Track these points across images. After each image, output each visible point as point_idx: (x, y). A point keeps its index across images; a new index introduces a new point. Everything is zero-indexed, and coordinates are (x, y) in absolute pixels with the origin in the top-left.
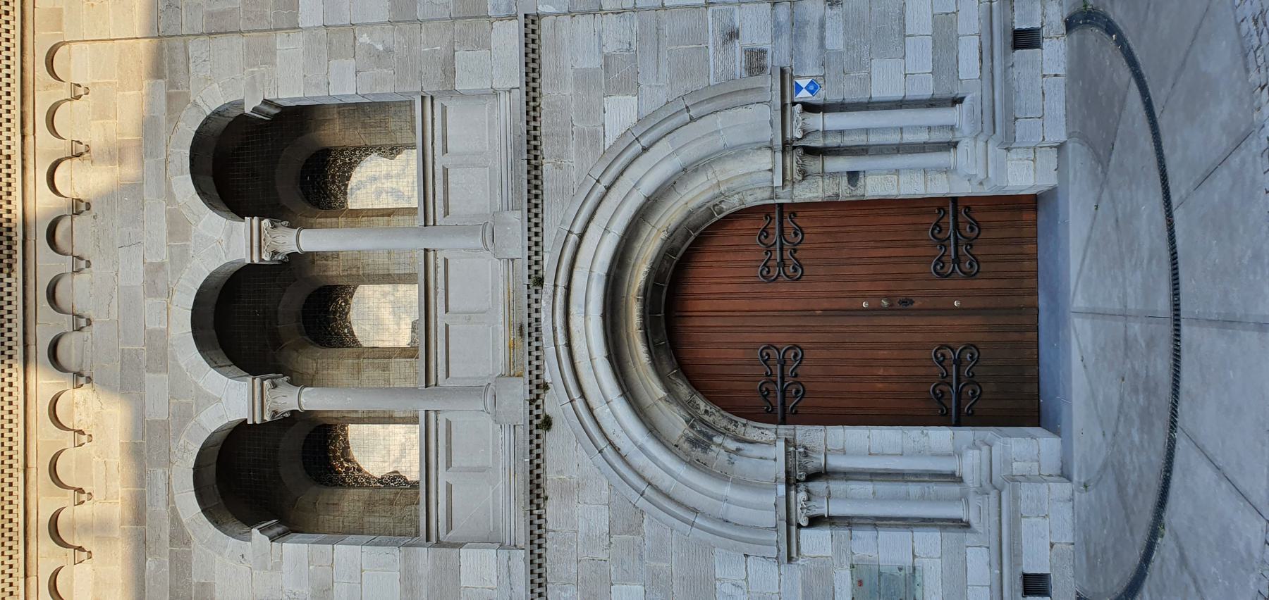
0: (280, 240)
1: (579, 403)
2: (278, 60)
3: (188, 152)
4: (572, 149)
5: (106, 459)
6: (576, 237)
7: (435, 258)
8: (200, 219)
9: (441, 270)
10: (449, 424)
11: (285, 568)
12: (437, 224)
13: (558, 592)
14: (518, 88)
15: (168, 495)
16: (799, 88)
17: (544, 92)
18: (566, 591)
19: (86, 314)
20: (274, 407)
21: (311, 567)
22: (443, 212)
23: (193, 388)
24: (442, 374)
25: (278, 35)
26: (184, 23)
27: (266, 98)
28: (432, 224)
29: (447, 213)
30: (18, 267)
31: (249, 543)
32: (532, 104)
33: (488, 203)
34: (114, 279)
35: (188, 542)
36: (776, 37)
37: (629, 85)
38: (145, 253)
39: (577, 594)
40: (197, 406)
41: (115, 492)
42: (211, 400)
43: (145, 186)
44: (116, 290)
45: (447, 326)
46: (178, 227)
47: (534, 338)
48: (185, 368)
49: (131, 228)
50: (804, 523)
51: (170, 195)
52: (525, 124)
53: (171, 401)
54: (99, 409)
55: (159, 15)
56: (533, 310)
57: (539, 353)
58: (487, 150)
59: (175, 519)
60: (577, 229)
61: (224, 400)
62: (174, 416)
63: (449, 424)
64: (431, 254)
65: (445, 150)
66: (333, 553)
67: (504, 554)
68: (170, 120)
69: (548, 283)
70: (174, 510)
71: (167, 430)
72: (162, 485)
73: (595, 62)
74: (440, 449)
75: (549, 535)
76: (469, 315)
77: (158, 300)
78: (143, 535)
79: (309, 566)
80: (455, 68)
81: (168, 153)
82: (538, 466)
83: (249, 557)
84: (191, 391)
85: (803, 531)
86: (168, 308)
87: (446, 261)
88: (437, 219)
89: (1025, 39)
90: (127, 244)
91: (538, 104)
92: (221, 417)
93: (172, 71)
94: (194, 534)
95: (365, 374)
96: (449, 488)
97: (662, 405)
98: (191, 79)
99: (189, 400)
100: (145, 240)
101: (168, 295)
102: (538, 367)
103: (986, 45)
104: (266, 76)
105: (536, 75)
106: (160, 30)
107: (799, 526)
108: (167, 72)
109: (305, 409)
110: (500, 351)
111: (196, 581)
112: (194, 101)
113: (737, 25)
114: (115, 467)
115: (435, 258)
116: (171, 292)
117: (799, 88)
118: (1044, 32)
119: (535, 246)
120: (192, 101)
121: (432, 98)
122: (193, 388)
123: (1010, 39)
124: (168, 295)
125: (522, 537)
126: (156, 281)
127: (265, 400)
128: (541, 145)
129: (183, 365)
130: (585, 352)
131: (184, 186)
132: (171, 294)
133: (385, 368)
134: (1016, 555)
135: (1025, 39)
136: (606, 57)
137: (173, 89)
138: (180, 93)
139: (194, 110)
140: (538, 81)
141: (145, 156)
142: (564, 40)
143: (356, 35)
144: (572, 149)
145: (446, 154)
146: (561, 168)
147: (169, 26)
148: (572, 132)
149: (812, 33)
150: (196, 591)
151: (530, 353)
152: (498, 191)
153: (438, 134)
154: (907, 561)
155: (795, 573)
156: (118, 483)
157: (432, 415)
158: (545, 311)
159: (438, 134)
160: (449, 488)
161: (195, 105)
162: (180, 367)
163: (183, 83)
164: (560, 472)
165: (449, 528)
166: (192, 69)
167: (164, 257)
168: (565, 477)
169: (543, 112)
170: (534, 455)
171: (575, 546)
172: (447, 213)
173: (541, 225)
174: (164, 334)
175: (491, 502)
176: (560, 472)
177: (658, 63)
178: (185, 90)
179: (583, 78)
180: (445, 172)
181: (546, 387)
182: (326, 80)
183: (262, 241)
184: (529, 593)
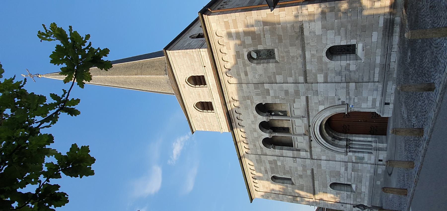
4: (314, 111)
16: (350, 106)
19: (244, 126)
29: (294, 115)
30: (234, 122)
36: (346, 100)
37: (323, 104)
46: (255, 117)
50: (348, 151)
51: (253, 113)
59: (260, 146)
69: (311, 127)
73: (318, 101)
85: (348, 153)
89: (388, 104)
95: (280, 122)
97: (329, 137)
103: (381, 103)
107: (348, 152)
113: (340, 98)
117: (350, 106)
118: (390, 103)
119: (309, 122)
123: (384, 104)
131: (255, 112)
133: (283, 121)
134: (378, 158)
135: (388, 104)
136: (319, 101)
144: (314, 111)
149: (352, 100)
154: (363, 156)
155: (347, 156)
167: (254, 120)
172: (294, 115)
177: (327, 102)
179: (316, 103)
181: (311, 137)
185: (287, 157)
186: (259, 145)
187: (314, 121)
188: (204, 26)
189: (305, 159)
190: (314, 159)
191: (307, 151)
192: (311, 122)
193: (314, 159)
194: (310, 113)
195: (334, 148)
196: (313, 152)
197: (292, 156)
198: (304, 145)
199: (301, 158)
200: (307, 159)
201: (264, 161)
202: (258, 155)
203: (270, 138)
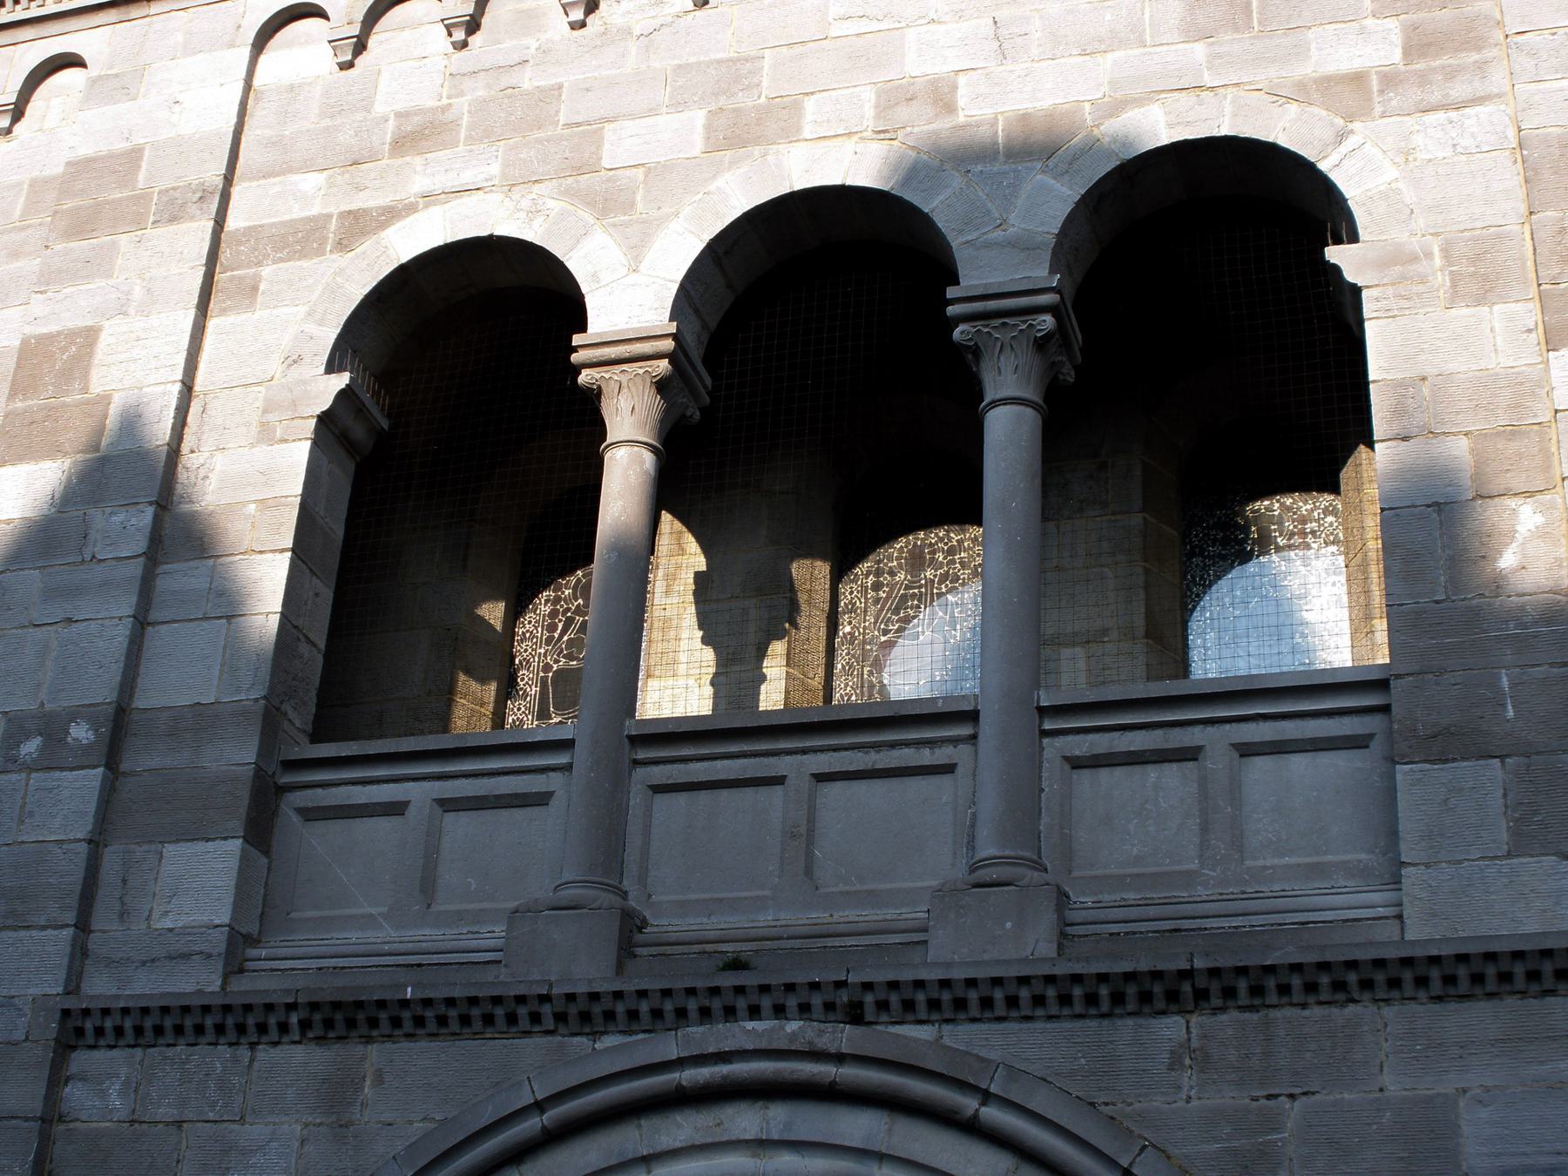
0: (1008, 362)
1: (531, 1126)
2: (1465, 311)
3: (1224, 131)
5: (531, 62)
6: (970, 1112)
7: (955, 741)
8: (1058, 176)
9: (926, 757)
10: (542, 799)
11: (263, 451)
12: (1046, 741)
13: (123, 1071)
14: (1403, 939)
15: (444, 193)
17: (1388, 1012)
18: (122, 1093)
20: (609, 391)
21: (253, 507)
22: (1077, 753)
23: (665, 210)
24: (660, 774)
25: (1531, 305)
26: (1541, 86)
27: (1365, 294)
28: (1047, 726)
29: (1076, 764)
31: (322, 369)
32: (1352, 978)
33: (1100, 872)
34: (920, 17)
35: (342, 246)
38: (979, 71)
39: (111, 1121)
40: (625, 225)
41: (462, 91)
42: (636, 252)
43: (1142, 50)
44: (897, 25)
45: (779, 780)
47: (706, 1003)
48: (712, 188)
49: (1038, 35)
52: (1293, 960)
53: (641, 170)
54: (637, 32)
55: (1561, 31)
56: (754, 998)
57: (669, 1016)
58: (1248, 863)
59: (391, 214)
60: (993, 1115)
61: (633, 278)
62: (608, 180)
63: (542, 799)
64: (964, 730)
65: (1247, 751)
66: (272, 551)
67: (218, 942)
68: (1301, 86)
69: (844, 1037)
70: (411, 209)
71: (579, 171)
72: (468, 177)
74: (485, 781)
75: (244, 1053)
76: (804, 835)
77: (869, 112)
78: (370, 156)
79: (255, 501)
80: (1454, 760)
81: (1222, 90)
82: (396, 1022)
83: (295, 373)
84: (659, 208)
86: (850, 134)
87: (949, 769)
88: (1060, 742)
90: (1003, 32)
91: (1356, 996)
92: (595, 276)
93: (1423, 79)
94: (357, 256)
96: (396, 809)
98: (1408, 118)
99: (640, 206)
100: (1010, 67)
101: (880, 132)
102: (633, 1015)
104: (1421, 288)
105: (1436, 987)
106: (1520, 38)
108: (1420, 66)
109: (607, 457)
110: (705, 920)
111: (263, 274)
112: (1352, 131)
114: (513, 82)
115: (955, 741)
116: (888, 136)
120: (1351, 126)
121: (1385, 709)
122: (665, 210)
124: (880, 132)
125: (258, 985)
126: (914, 102)
127: (625, 367)
128: (1320, 1003)
129: (720, 182)
130: (666, 1141)
132: (882, 136)
137: (1381, 82)
138: (1370, 100)
139: (1328, 135)
140: (1422, 994)
141: (1212, 44)
142: (1542, 1063)
143: (1539, 497)
145: (1236, 755)
146: (1171, 1068)
147: (1533, 54)
148: (1276, 1096)
150: (240, 278)
151: (667, 993)
152: (1131, 896)
153: (1291, 730)
156: (480, 94)
157: (561, 759)
158: (773, 1029)
159: (1291, 730)
160: (396, 809)
161: (1341, 137)
162: (714, 177)
163: (1394, 103)
164: (379, 1079)
165: (311, 814)
166: (1431, 118)
168: (366, 1090)
169: (1335, 1011)
170: (419, 1011)
171: (211, 1116)
172: (1076, 764)
173: (1066, 1011)
174: (791, 133)
175: (354, 911)
176: (379, 1079)
178: (1378, 109)
180: (1189, 755)
182: (1415, 431)
183: (1001, 321)
184: (122, 1005)
185: (141, 623)
186: (429, 198)
187: (986, 1097)
188: (608, 1086)
189: (83, 926)
190: (57, 1079)
191: (234, 965)
192: (963, 1036)
193: (57, 1079)
194: (1171, 1028)
195: (1071, 324)
196: (217, 1058)
197: (140, 702)
198: (369, 921)
199: (96, 844)
200: (80, 953)
201: (96, 266)
202: (229, 179)
203: (575, 358)
